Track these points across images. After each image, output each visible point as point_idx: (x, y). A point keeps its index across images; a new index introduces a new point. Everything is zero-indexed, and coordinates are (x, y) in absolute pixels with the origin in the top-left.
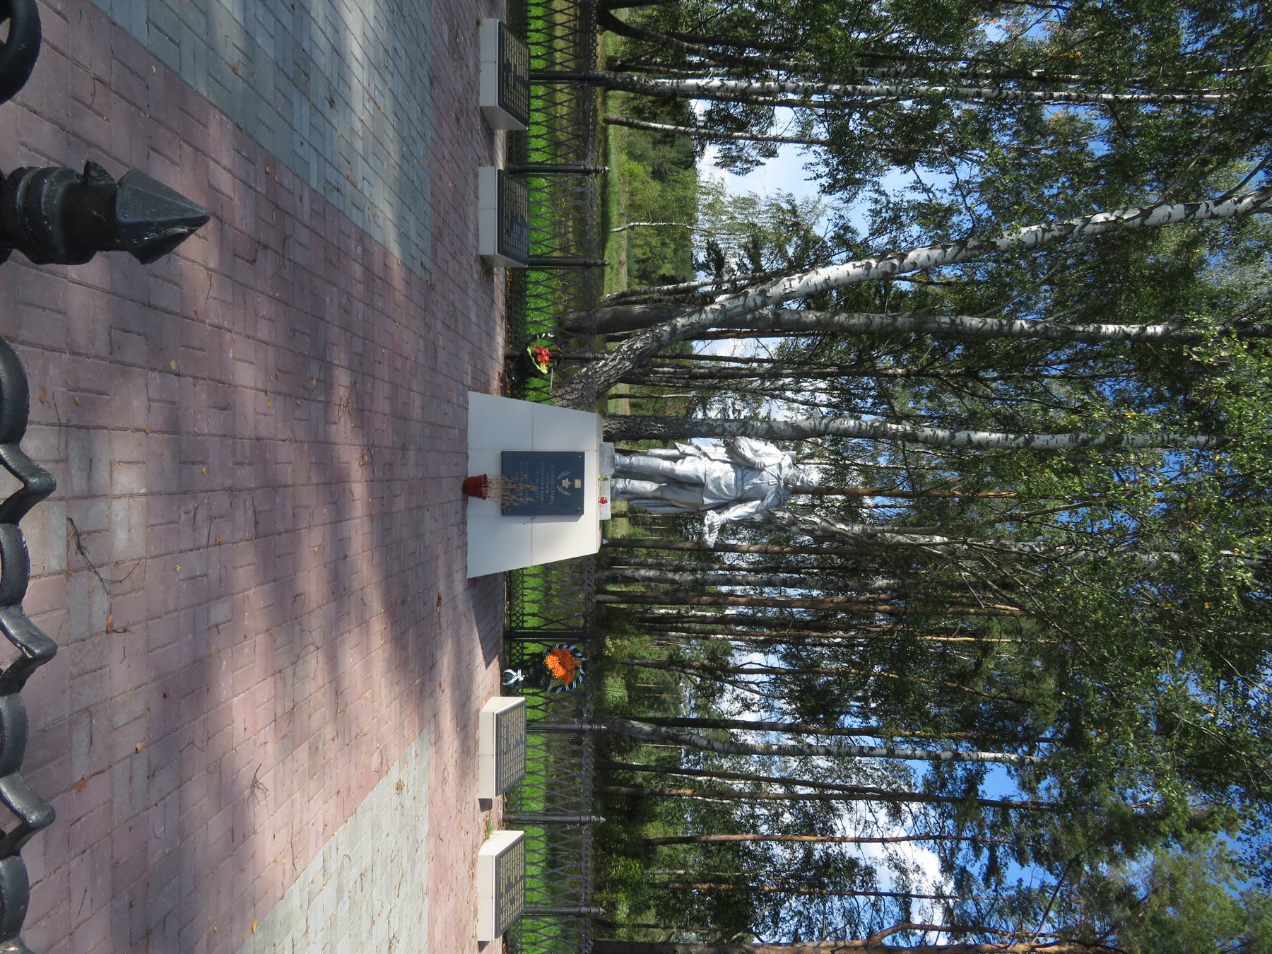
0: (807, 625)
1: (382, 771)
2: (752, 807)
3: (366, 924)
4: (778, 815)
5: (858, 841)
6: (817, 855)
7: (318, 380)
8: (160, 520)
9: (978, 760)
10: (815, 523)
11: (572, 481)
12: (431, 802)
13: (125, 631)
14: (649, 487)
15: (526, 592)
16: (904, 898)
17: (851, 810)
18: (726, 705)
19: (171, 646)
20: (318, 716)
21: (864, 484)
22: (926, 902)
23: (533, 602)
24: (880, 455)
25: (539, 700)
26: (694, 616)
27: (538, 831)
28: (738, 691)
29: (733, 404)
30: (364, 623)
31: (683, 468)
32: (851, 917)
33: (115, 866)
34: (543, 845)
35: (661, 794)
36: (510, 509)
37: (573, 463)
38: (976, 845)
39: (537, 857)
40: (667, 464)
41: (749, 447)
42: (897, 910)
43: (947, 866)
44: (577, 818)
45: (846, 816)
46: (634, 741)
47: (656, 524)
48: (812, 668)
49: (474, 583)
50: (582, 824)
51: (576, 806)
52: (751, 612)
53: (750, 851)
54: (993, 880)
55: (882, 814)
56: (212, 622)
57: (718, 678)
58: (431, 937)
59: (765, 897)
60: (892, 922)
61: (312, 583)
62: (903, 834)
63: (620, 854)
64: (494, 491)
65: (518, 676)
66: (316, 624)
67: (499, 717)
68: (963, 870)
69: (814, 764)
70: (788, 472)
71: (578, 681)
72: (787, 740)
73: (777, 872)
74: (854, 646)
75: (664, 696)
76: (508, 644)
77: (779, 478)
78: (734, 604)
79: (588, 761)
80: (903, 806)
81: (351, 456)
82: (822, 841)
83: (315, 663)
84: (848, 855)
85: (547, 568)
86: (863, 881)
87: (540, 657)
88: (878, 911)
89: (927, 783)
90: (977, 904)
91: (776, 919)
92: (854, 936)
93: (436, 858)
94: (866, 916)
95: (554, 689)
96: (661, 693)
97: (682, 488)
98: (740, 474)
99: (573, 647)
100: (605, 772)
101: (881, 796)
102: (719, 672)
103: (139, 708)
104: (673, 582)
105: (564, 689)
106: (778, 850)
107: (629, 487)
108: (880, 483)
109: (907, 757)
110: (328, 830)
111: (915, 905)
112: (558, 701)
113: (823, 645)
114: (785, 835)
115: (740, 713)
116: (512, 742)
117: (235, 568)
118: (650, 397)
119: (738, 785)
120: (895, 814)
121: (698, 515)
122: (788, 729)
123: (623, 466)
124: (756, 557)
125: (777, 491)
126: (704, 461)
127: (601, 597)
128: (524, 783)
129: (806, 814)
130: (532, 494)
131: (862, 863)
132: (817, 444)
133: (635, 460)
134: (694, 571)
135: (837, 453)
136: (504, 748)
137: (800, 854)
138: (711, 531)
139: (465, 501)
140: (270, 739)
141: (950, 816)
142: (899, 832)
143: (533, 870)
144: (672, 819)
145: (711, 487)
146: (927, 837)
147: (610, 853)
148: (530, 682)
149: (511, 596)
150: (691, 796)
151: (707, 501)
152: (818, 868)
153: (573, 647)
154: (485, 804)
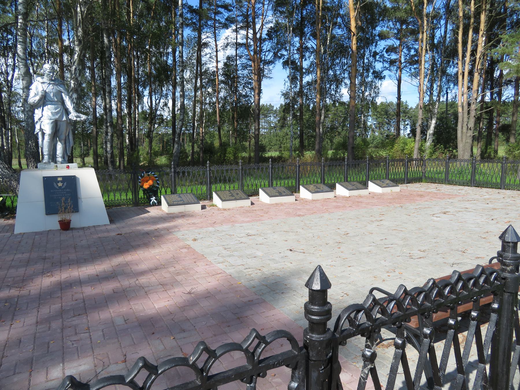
0: (130, 76)
1: (188, 247)
2: (206, 104)
3: (242, 244)
4: (209, 94)
5: (217, 62)
6: (223, 79)
7: (6, 303)
8: (76, 354)
9: (182, 6)
10: (75, 69)
11: (59, 182)
12: (201, 228)
13: (125, 355)
14: (59, 147)
15: (116, 199)
16: (238, 45)
17: (206, 64)
18: (166, 114)
19: (133, 336)
20: (165, 275)
21: (57, 44)
22: (239, 36)
23: (121, 195)
24: (41, 35)
25: (163, 190)
26: (129, 127)
27: (213, 187)
28: (159, 108)
29: (19, 107)
30: (127, 264)
31: (48, 129)
32: (245, 67)
33: (215, 335)
34: (218, 185)
35: (202, 140)
36: (75, 208)
37: (49, 183)
38: (217, 13)
39: (223, 186)
40: (47, 138)
41: (33, 98)
42: (242, 49)
43: (226, 26)
44: (208, 172)
45: (208, 66)
46: (182, 153)
47: (87, 145)
48: (149, 75)
49: (112, 221)
50: (210, 170)
51: (204, 174)
52: (125, 102)
53: (223, 105)
54: (230, 8)
55: (207, 50)
56: (124, 323)
57: (155, 116)
58: (249, 222)
59: (238, 101)
60: (246, 51)
61: (108, 287)
62: (214, 43)
63: (225, 156)
64: (67, 217)
65: (153, 199)
66: (126, 283)
67: (170, 205)
68: (226, 19)
69: (188, 77)
70: (46, 79)
71: (154, 175)
72: (178, 89)
73: (230, 95)
74: (138, 56)
75: (165, 140)
76: (141, 204)
77: (50, 84)
78: (122, 110)
79: (190, 169)
80: (203, 41)
81: (47, 281)
82: (218, 76)
83: (143, 280)
84: (223, 66)
85: (105, 190)
86: (232, 61)
87: (145, 190)
88: (242, 56)
89: (194, 30)
90: (238, 16)
91: (246, 96)
92: (251, 66)
93: (222, 223)
94: (244, 60)
95: (158, 184)
96: (164, 141)
97: (59, 130)
98: (48, 103)
99: (140, 177)
100: (195, 163)
101: (199, 50)
102: (152, 116)
103: (158, 342)
104: (112, 136)
105: (158, 180)
106: (222, 94)
107: (60, 155)
108: (56, 37)
109: (183, 36)
110: (209, 264)
111: (240, 41)
112: (163, 182)
113: (138, 71)
114: (216, 91)
115: (169, 108)
116: (179, 199)
117: (100, 319)
118: (19, 149)
119: (198, 109)
120: (206, 45)
121: (74, 124)
122: (174, 88)
123: (49, 158)
124: (99, 98)
125: (57, 85)
126: (45, 119)
127: (122, 168)
128: (196, 193)
129: (208, 82)
130: (66, 200)
131: (225, 61)
132: (37, 66)
133: (46, 152)
134: (107, 127)
135: (41, 56)
136: (182, 202)
137: (222, 85)
138: (80, 117)
139: (73, 229)
140: (173, 291)
141: (206, 22)
142: (213, 44)
143: (227, 187)
144: (212, 136)
145: (57, 117)
146: (215, 33)
147: (225, 160)
148: (155, 194)
149: (119, 205)
150: (202, 128)
151: (64, 119)
152: (228, 79)
153: (140, 177)
154: (203, 207)
